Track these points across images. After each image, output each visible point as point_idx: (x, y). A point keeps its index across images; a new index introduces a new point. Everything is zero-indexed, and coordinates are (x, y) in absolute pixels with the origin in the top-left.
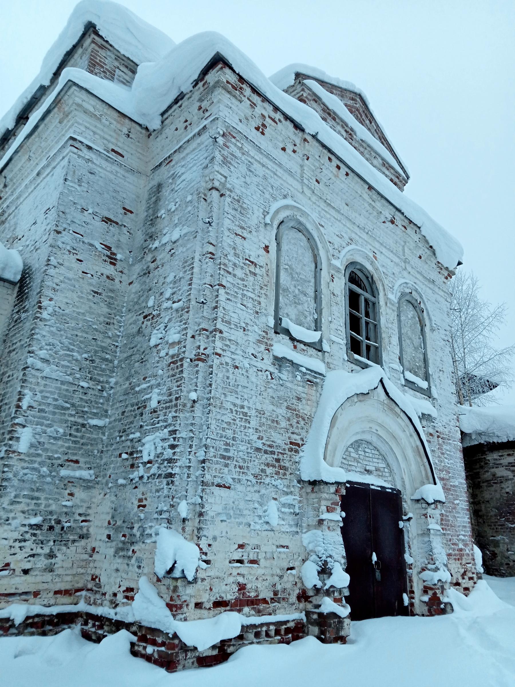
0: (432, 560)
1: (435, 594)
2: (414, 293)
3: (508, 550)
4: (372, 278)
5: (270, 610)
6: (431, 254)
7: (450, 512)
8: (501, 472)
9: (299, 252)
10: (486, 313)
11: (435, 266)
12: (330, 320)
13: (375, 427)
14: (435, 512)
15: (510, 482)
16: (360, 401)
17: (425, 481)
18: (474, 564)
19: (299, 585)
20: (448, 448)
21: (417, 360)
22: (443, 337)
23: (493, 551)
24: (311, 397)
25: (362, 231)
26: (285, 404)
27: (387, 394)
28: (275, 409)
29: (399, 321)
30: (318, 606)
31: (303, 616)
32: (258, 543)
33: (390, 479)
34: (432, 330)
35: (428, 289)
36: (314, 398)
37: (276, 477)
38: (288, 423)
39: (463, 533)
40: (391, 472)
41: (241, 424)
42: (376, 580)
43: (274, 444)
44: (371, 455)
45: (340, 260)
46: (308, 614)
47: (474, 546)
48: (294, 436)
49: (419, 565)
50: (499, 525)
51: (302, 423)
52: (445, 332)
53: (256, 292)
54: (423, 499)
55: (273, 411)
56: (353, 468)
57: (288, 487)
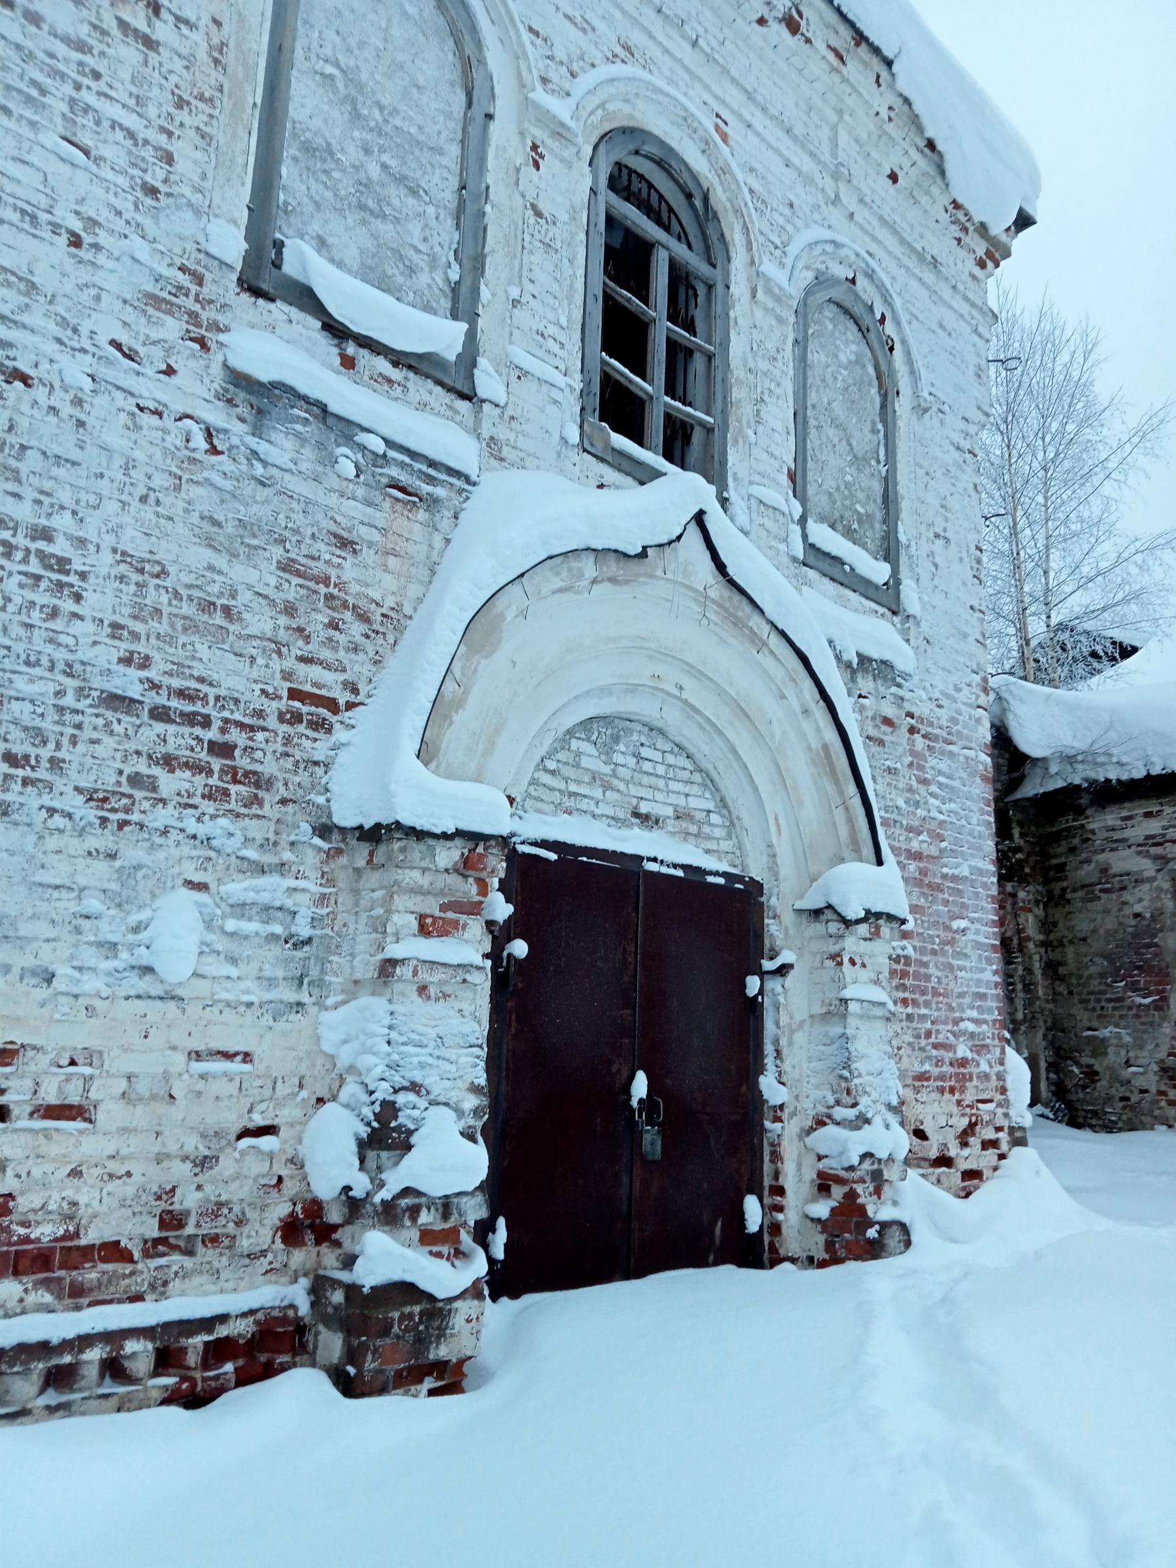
0: (847, 1093)
1: (852, 1195)
2: (861, 282)
3: (1128, 1064)
4: (706, 199)
5: (140, 1283)
6: (932, 171)
7: (934, 953)
8: (1124, 861)
9: (395, 32)
10: (1114, 430)
11: (945, 218)
12: (514, 293)
13: (671, 677)
14: (881, 951)
15: (1147, 886)
16: (613, 580)
17: (846, 854)
18: (1005, 1104)
19: (291, 1188)
20: (943, 766)
21: (861, 495)
22: (957, 438)
23: (1089, 1066)
24: (401, 546)
25: (674, 33)
26: (277, 552)
27: (721, 567)
28: (221, 562)
29: (802, 362)
30: (349, 1262)
31: (299, 1296)
32: (95, 1043)
33: (726, 845)
34: (921, 410)
35: (914, 284)
36: (418, 551)
37: (209, 807)
38: (283, 620)
39: (974, 1014)
40: (732, 824)
41: (30, 595)
42: (642, 1157)
43: (204, 688)
44: (661, 770)
45: (572, 102)
46: (319, 1286)
47: (1010, 1052)
48: (315, 672)
49: (810, 1108)
50: (1110, 1000)
51: (356, 629)
52: (962, 425)
53: (152, 111)
54: (829, 906)
55: (211, 568)
56: (584, 804)
57: (267, 845)
